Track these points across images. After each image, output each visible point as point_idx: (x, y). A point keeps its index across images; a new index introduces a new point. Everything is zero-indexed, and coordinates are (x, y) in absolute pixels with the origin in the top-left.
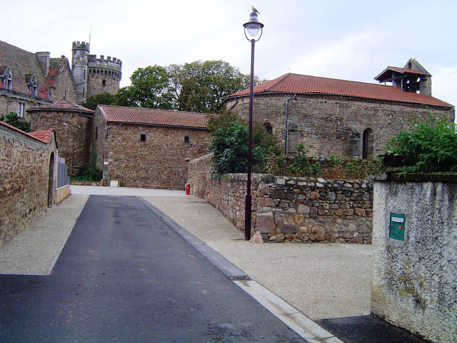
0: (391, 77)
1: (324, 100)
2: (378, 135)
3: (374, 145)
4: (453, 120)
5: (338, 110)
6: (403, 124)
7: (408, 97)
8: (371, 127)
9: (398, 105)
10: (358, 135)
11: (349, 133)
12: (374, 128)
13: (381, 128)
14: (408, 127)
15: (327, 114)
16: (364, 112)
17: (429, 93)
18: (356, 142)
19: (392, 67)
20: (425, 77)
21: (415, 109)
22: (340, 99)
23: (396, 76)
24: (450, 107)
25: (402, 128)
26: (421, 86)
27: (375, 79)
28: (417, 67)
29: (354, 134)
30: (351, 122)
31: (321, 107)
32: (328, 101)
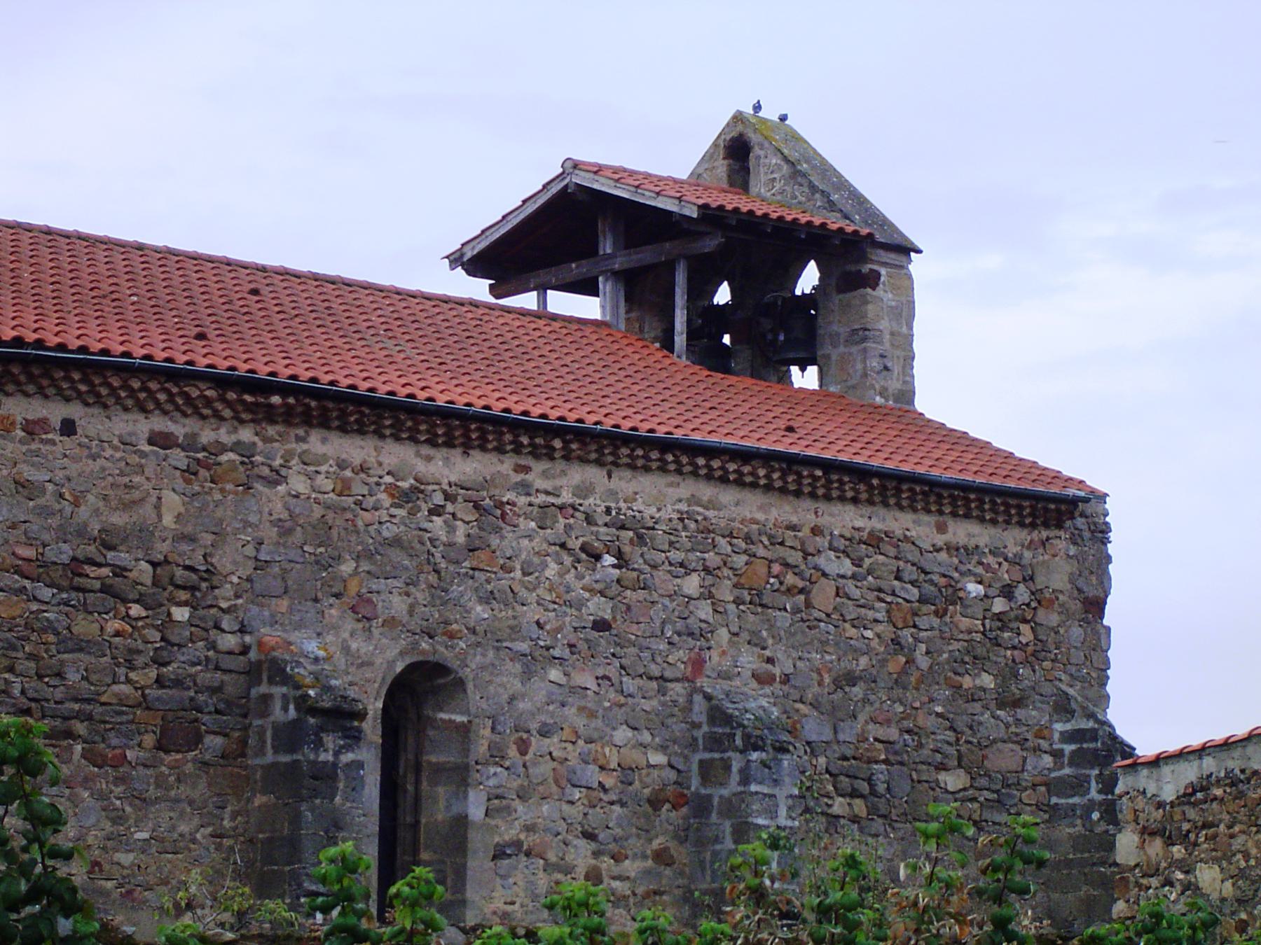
0: (591, 251)
1: (56, 412)
2: (507, 725)
3: (476, 811)
4: (1096, 606)
5: (173, 501)
6: (703, 634)
7: (730, 413)
8: (446, 655)
9: (663, 469)
10: (342, 717)
11: (266, 699)
12: (471, 662)
13: (531, 664)
14: (749, 660)
15: (81, 532)
16: (391, 521)
17: (894, 385)
18: (325, 776)
19: (598, 170)
20: (862, 253)
21: (801, 513)
22: (193, 408)
23: (630, 241)
24: (1074, 502)
25: (698, 664)
26: (834, 324)
27: (456, 260)
28: (796, 174)
29: (314, 711)
30: (284, 604)
31: (28, 472)
32: (91, 422)
